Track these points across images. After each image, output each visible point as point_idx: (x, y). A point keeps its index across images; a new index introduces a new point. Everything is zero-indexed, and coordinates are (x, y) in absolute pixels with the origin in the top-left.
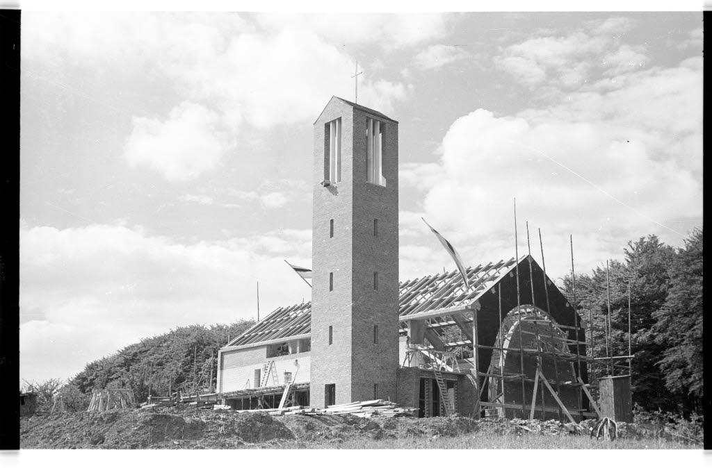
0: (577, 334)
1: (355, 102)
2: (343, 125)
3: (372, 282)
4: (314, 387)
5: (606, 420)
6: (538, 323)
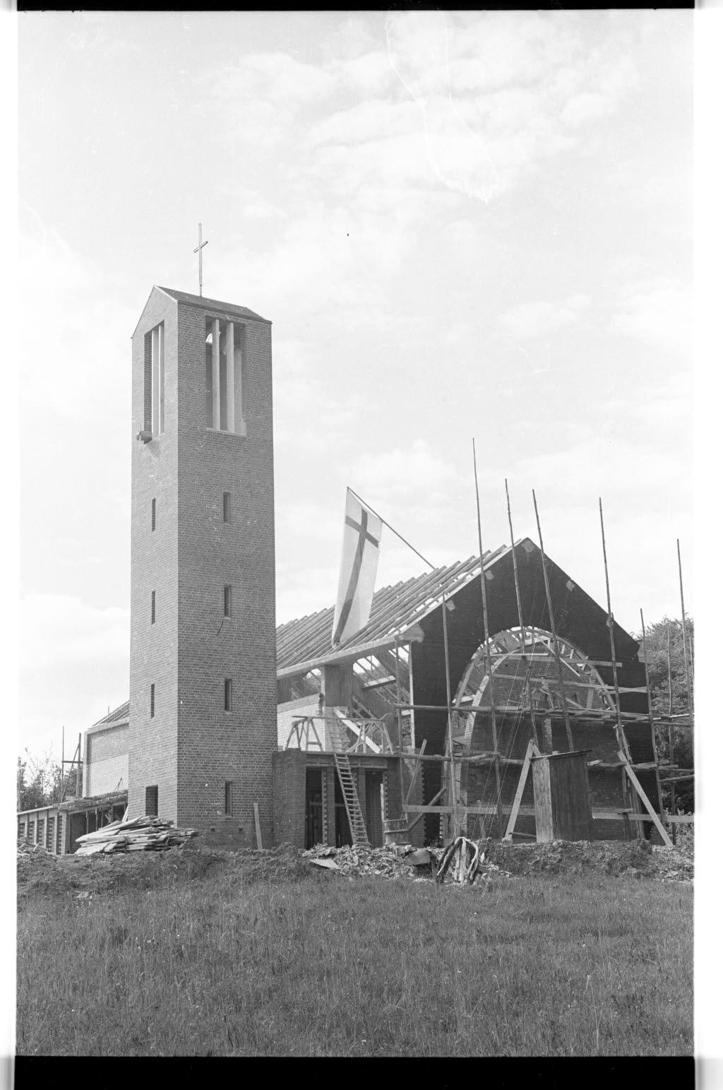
0: (615, 673)
1: (198, 294)
2: (166, 334)
3: (221, 603)
4: (302, 786)
5: (461, 842)
6: (528, 659)
